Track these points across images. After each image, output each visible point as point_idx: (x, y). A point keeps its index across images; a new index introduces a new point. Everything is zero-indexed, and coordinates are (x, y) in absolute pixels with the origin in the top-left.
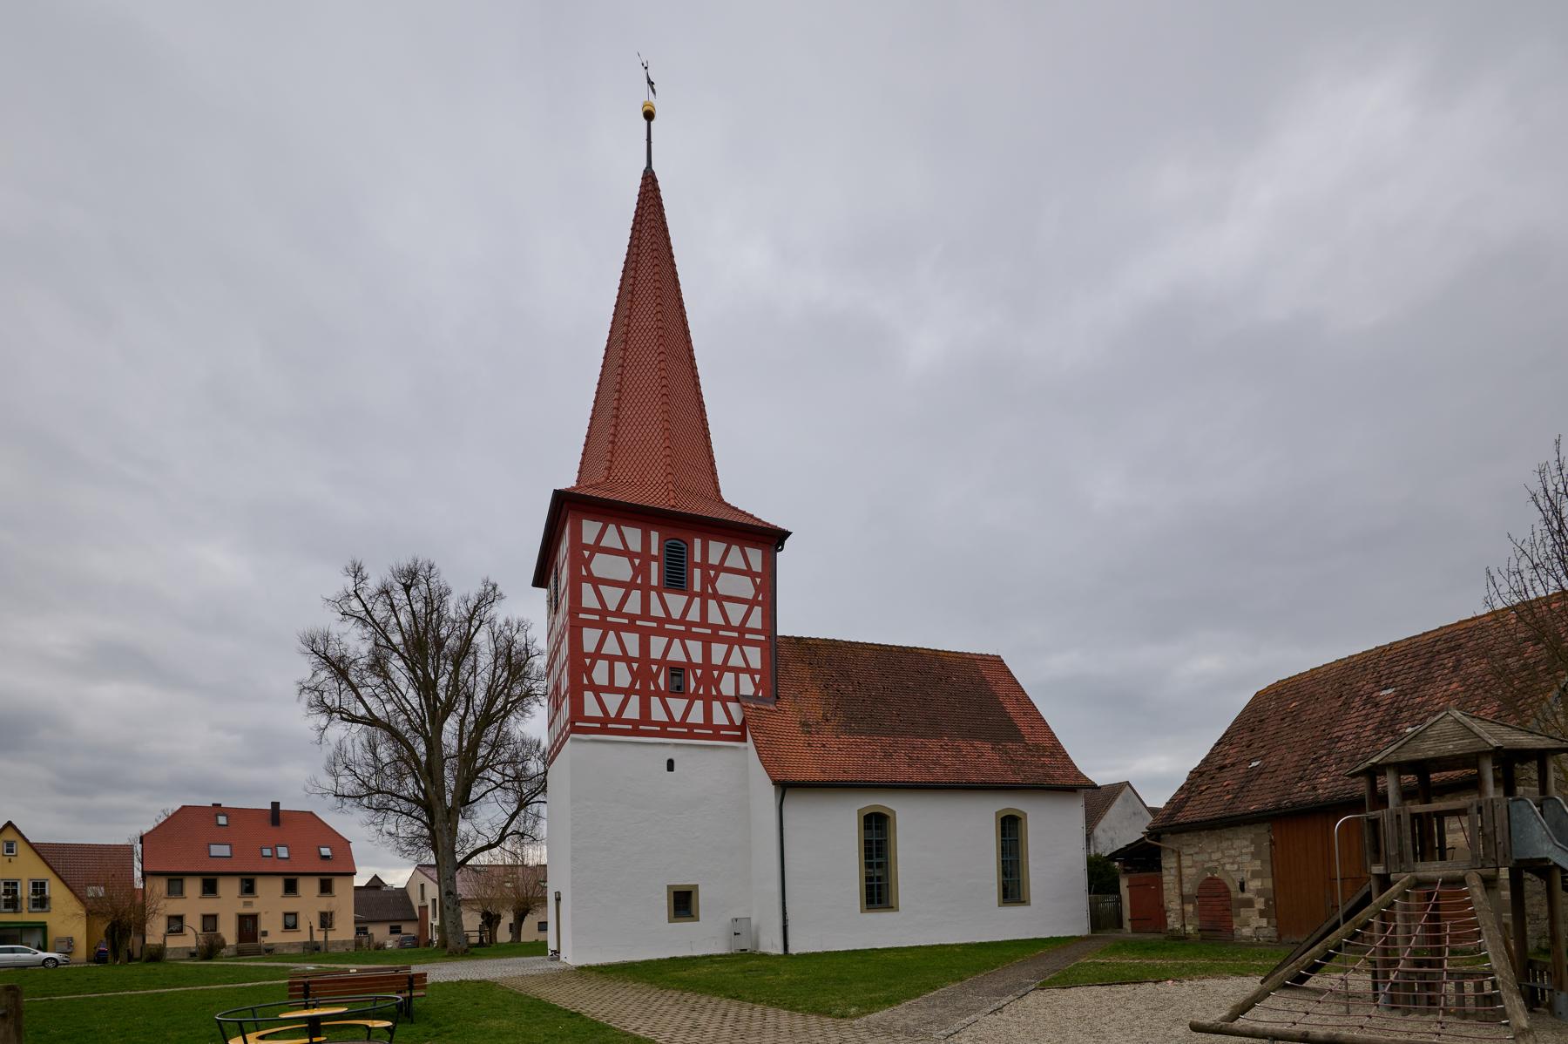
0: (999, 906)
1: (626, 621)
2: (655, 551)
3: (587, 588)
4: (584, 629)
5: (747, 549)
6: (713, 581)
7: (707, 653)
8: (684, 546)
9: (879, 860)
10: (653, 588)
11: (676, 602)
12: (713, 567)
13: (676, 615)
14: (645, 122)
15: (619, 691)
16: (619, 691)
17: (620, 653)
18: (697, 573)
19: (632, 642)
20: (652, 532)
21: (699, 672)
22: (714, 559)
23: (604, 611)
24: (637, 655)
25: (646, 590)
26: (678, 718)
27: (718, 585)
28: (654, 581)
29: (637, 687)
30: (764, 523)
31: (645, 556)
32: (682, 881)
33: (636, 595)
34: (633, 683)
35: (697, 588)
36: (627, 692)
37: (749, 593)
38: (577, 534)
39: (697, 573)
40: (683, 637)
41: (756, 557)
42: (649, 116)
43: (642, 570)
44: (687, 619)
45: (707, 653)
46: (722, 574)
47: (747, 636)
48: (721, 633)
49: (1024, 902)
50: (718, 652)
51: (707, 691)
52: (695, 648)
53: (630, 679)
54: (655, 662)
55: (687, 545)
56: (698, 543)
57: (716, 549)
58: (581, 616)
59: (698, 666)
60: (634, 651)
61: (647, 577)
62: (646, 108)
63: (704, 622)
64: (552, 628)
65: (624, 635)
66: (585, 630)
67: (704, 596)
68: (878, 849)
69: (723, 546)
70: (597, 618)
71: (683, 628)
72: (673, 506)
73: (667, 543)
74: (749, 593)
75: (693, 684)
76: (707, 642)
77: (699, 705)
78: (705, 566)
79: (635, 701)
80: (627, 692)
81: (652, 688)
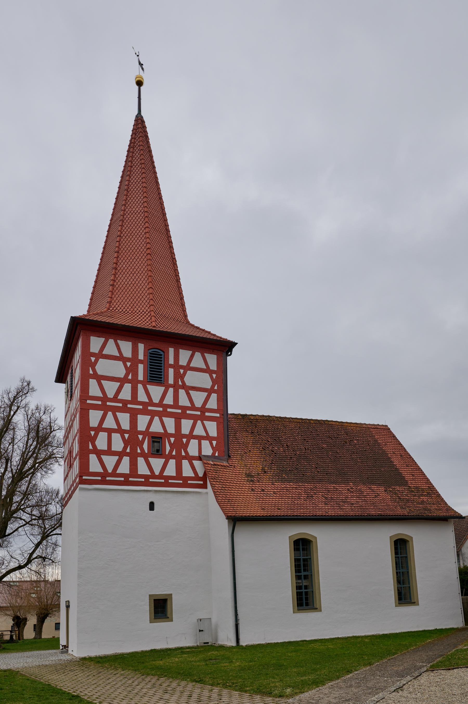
2: (141, 357)
3: (93, 383)
6: (182, 377)
7: (178, 426)
8: (162, 353)
9: (306, 573)
12: (182, 367)
13: (156, 400)
14: (137, 87)
18: (171, 371)
21: (172, 440)
22: (183, 361)
23: (105, 398)
25: (135, 383)
26: (157, 473)
27: (185, 379)
28: (141, 377)
29: (128, 450)
30: (218, 337)
31: (134, 360)
32: (161, 591)
33: (128, 387)
34: (125, 448)
35: (171, 381)
36: (191, 436)
38: (86, 346)
39: (171, 371)
40: (161, 415)
41: (212, 360)
42: (140, 83)
43: (132, 370)
45: (178, 426)
47: (207, 414)
48: (188, 412)
49: (414, 603)
50: (186, 425)
51: (179, 452)
52: (170, 423)
54: (141, 433)
55: (164, 352)
56: (171, 351)
57: (184, 355)
58: (89, 402)
59: (172, 435)
60: (126, 425)
61: (136, 374)
62: (138, 79)
63: (176, 405)
64: (68, 411)
67: (176, 387)
68: (304, 566)
70: (100, 403)
71: (161, 409)
72: (154, 327)
73: (150, 351)
75: (168, 448)
76: (178, 419)
77: (172, 463)
78: (176, 366)
79: (126, 460)
81: (139, 451)
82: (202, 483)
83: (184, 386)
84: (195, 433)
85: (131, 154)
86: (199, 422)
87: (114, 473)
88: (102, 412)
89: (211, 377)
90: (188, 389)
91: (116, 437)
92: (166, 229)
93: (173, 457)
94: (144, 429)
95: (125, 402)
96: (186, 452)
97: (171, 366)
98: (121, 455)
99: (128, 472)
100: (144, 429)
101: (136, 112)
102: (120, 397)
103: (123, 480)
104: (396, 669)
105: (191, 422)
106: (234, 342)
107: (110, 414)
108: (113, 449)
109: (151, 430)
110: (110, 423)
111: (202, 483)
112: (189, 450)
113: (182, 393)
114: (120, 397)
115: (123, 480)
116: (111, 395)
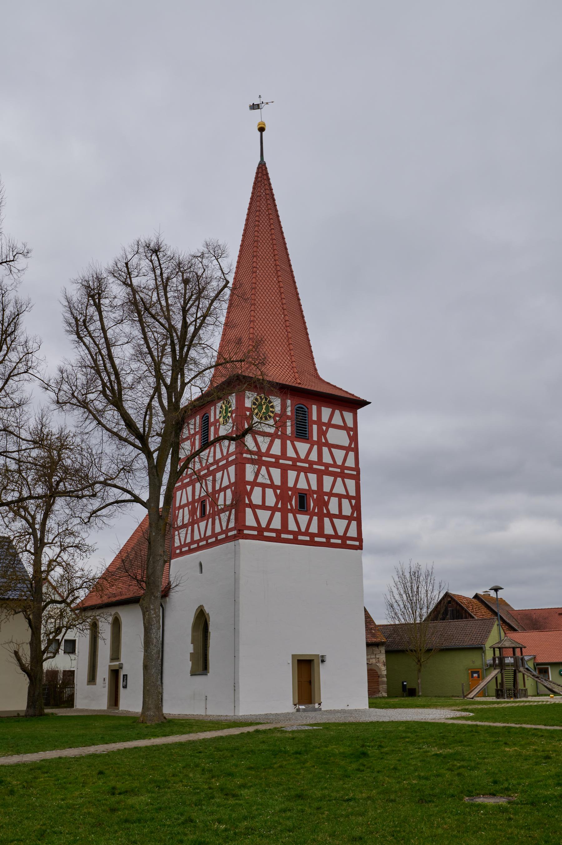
0: (95, 684)
1: (273, 460)
4: (289, 471)
5: (344, 413)
7: (320, 483)
8: (306, 409)
10: (289, 438)
11: (303, 447)
12: (324, 424)
14: (259, 133)
15: (345, 517)
16: (345, 517)
18: (315, 427)
19: (276, 473)
20: (313, 406)
21: (315, 496)
22: (325, 419)
23: (259, 453)
24: (279, 484)
27: (328, 436)
29: (279, 506)
30: (350, 394)
33: (278, 443)
34: (277, 503)
35: (315, 438)
37: (346, 442)
39: (315, 427)
40: (306, 471)
41: (348, 416)
42: (262, 130)
43: (280, 424)
45: (320, 483)
46: (330, 429)
47: (346, 471)
48: (315, 466)
50: (328, 481)
51: (321, 510)
52: (313, 478)
53: (350, 511)
54: (290, 489)
56: (314, 408)
57: (326, 412)
59: (314, 492)
60: (277, 481)
62: (261, 126)
63: (320, 461)
67: (320, 446)
69: (330, 410)
71: (307, 465)
72: (300, 383)
74: (346, 442)
76: (320, 475)
78: (319, 422)
82: (282, 535)
83: (327, 444)
86: (339, 480)
89: (349, 435)
90: (331, 447)
93: (315, 514)
94: (328, 491)
95: (277, 457)
97: (315, 422)
98: (273, 510)
99: (279, 528)
100: (328, 491)
101: (259, 160)
103: (257, 534)
104: (265, 755)
108: (343, 514)
109: (298, 487)
111: (282, 535)
112: (252, 498)
113: (325, 450)
115: (257, 534)
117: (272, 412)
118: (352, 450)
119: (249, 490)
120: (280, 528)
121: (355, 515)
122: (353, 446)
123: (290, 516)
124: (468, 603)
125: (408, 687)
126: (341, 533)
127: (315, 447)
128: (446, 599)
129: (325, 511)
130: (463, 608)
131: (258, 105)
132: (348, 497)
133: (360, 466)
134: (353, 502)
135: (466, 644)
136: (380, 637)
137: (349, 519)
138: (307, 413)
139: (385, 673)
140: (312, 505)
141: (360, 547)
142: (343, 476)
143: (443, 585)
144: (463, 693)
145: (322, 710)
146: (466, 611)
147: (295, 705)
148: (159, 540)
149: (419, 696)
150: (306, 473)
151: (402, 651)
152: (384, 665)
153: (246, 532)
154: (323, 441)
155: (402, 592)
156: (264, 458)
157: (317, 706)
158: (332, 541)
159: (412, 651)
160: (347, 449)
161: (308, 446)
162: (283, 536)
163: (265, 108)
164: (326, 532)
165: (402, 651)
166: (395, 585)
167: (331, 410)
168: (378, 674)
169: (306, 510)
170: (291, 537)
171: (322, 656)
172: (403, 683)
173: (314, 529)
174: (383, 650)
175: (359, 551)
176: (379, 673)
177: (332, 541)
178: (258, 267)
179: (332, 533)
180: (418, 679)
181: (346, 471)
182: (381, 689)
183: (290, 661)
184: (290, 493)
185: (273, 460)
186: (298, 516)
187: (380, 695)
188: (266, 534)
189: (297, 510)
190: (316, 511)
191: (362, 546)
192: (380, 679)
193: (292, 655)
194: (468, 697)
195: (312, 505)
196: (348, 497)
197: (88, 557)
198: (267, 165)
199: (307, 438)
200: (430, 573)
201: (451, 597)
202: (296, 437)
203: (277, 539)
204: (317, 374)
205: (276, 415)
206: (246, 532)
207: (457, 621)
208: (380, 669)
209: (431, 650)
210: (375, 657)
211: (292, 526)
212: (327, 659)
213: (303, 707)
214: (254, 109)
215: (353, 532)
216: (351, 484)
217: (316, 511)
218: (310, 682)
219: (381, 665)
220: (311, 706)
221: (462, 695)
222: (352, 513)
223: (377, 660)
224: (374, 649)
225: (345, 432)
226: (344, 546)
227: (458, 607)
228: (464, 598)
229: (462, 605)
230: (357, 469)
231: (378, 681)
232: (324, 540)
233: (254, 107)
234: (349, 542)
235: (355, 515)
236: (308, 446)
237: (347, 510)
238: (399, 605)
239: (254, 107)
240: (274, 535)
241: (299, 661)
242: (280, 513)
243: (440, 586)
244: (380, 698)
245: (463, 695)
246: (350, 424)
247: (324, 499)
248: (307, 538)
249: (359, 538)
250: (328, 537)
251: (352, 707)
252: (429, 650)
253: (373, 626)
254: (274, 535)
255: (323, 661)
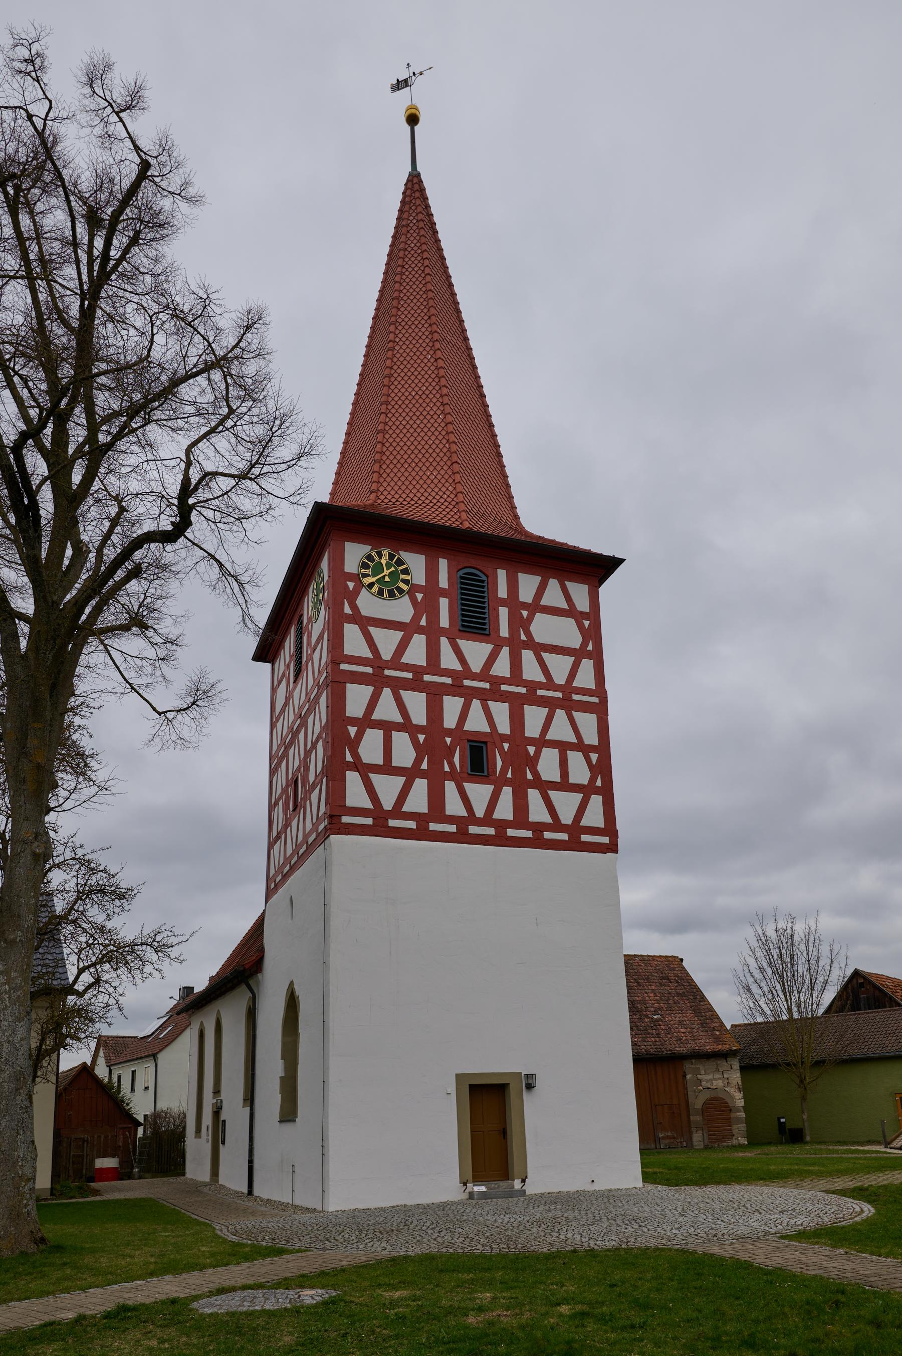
1: (409, 675)
2: (444, 583)
3: (352, 632)
4: (445, 697)
5: (570, 585)
6: (526, 624)
7: (517, 720)
8: (484, 578)
10: (443, 632)
12: (525, 606)
13: (476, 666)
14: (408, 128)
17: (399, 719)
18: (503, 612)
20: (499, 571)
21: (506, 746)
23: (376, 661)
24: (424, 723)
25: (433, 634)
27: (533, 628)
28: (444, 622)
29: (424, 766)
31: (432, 590)
34: (418, 761)
35: (504, 632)
37: (575, 640)
38: (338, 562)
39: (503, 612)
40: (485, 697)
41: (579, 593)
42: (413, 119)
43: (428, 607)
44: (402, 661)
45: (517, 720)
47: (575, 697)
48: (540, 692)
50: (534, 718)
51: (519, 773)
52: (501, 711)
53: (588, 774)
54: (449, 732)
55: (487, 577)
56: (502, 575)
57: (528, 585)
58: (343, 666)
59: (504, 738)
60: (419, 717)
62: (410, 111)
65: (405, 694)
66: (349, 686)
67: (516, 647)
69: (536, 580)
70: (370, 670)
71: (486, 685)
73: (461, 573)
74: (575, 640)
78: (513, 601)
79: (421, 786)
80: (410, 774)
84: (375, 716)
85: (404, 230)
86: (560, 714)
87: (397, 812)
88: (371, 689)
89: (580, 627)
90: (539, 649)
91: (401, 740)
92: (469, 355)
93: (507, 783)
94: (536, 735)
95: (417, 670)
96: (536, 774)
97: (503, 602)
99: (425, 810)
100: (536, 735)
102: (405, 659)
103: (371, 823)
105: (544, 711)
106: (614, 558)
107: (387, 692)
108: (572, 780)
109: (467, 727)
110: (386, 709)
113: (528, 656)
114: (405, 659)
115: (371, 823)
116: (387, 654)
117: (406, 582)
118: (589, 655)
119: (353, 735)
120: (426, 811)
121: (599, 783)
122: (590, 648)
123: (450, 787)
124: (895, 986)
125: (788, 1126)
126: (567, 818)
127: (505, 651)
128: (855, 981)
129: (529, 776)
130: (885, 994)
131: (406, 81)
132: (580, 746)
133: (608, 687)
134: (594, 757)
135: (887, 1051)
136: (730, 1043)
137: (587, 791)
138: (485, 584)
139: (741, 1103)
140: (499, 763)
141: (613, 848)
142: (569, 706)
143: (836, 948)
144: (884, 1136)
145: (527, 1193)
146: (891, 998)
147: (465, 1184)
148: (21, 806)
149: (806, 1143)
150: (484, 702)
151: (772, 1067)
152: (739, 1089)
153: (345, 819)
154: (523, 637)
155: (765, 965)
156: (387, 672)
157: (517, 1184)
158: (547, 835)
159: (788, 1064)
160: (578, 655)
161: (489, 647)
162: (433, 827)
163: (418, 82)
164: (533, 818)
165: (772, 1067)
166: (751, 954)
167: (538, 579)
168: (729, 1107)
169: (486, 774)
170: (452, 828)
171: (527, 1076)
172: (779, 1119)
173: (505, 810)
174: (736, 1065)
175: (609, 855)
176: (730, 1105)
177: (547, 835)
178: (397, 340)
179: (547, 818)
180: (803, 1113)
181: (575, 697)
182: (735, 1132)
183: (452, 1089)
184: (448, 740)
185: (409, 675)
186: (467, 786)
187: (735, 1142)
188: (392, 823)
189: (466, 775)
190: (509, 775)
191: (617, 845)
192: (733, 1115)
193: (457, 1075)
194: (892, 1146)
195: (499, 763)
196: (580, 746)
197: (127, 908)
198: (423, 177)
199: (487, 632)
200: (813, 929)
201: (864, 978)
202: (460, 630)
203: (422, 834)
204: (519, 524)
205: (414, 589)
206: (345, 819)
207: (871, 1013)
208: (732, 1097)
209: (824, 1062)
210: (721, 1076)
211: (454, 806)
212: (539, 1082)
213: (483, 1189)
214: (399, 90)
215: (594, 816)
216: (587, 723)
217: (509, 775)
218: (504, 1133)
219: (733, 1090)
220: (504, 1184)
221: (881, 1139)
222: (593, 780)
223: (726, 1081)
224: (719, 1062)
225: (572, 621)
226: (574, 844)
227: (877, 993)
228: (888, 978)
229: (884, 989)
230: (600, 690)
231: (730, 1118)
232: (528, 834)
233: (401, 85)
234: (585, 838)
235: (599, 783)
236: (489, 647)
237: (579, 772)
238: (761, 987)
239: (401, 85)
240: (412, 825)
241: (473, 1087)
242: (426, 781)
243: (831, 950)
244: (734, 1146)
245: (885, 1141)
246: (583, 605)
247: (527, 752)
248: (491, 831)
249: (610, 828)
250: (538, 828)
251: (602, 1185)
252: (819, 1064)
253: (717, 1025)
254: (412, 825)
255: (530, 1087)
